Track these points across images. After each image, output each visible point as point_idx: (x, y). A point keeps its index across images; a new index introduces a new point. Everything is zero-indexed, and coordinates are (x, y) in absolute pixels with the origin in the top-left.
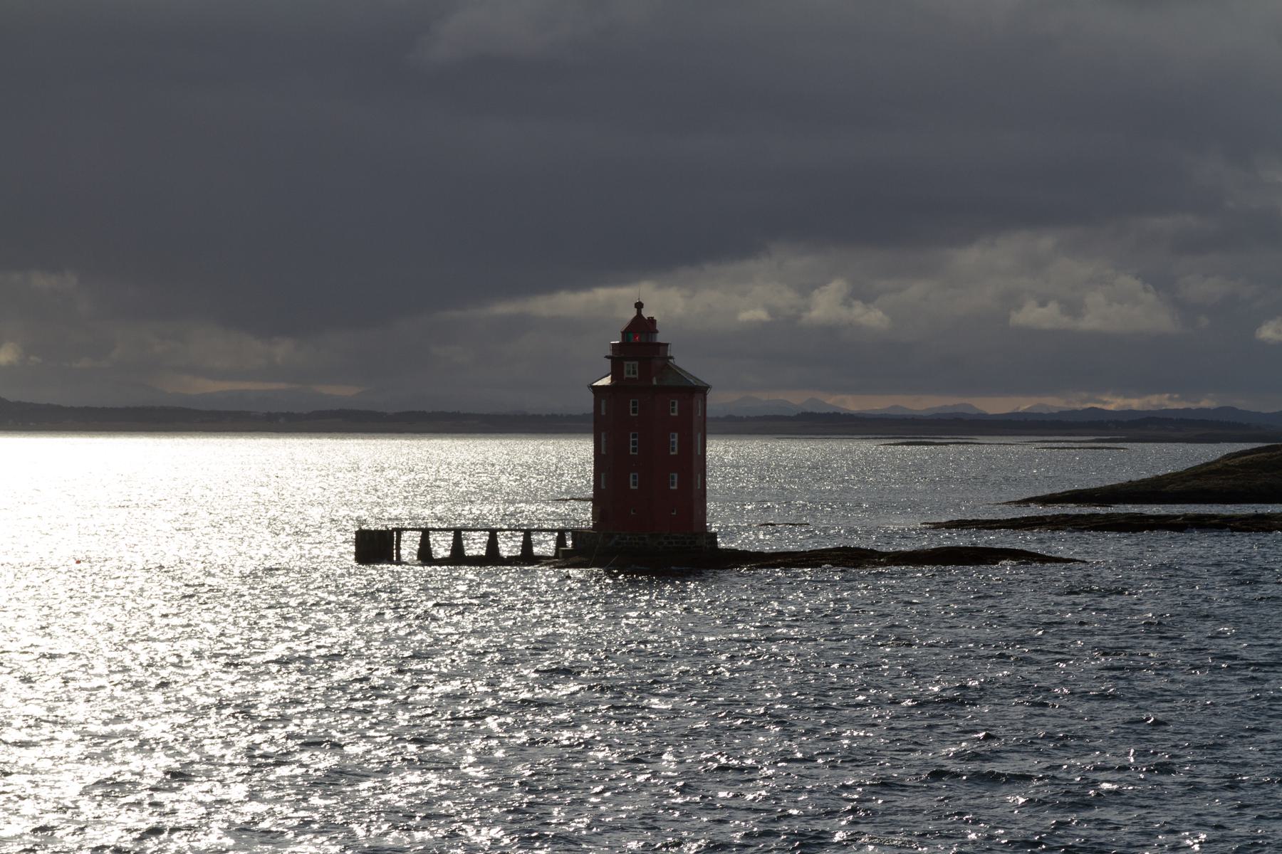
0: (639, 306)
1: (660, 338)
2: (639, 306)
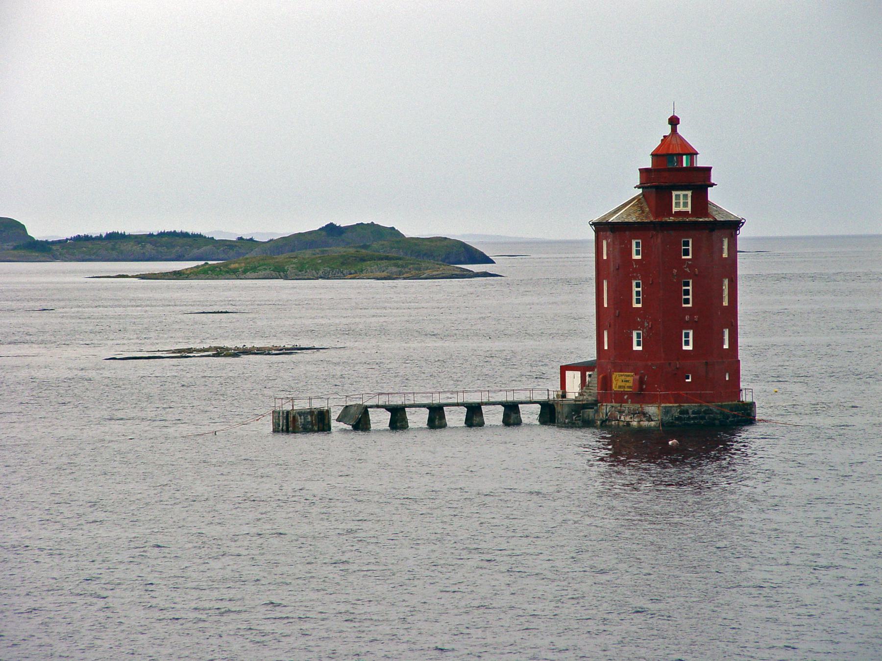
0: (674, 121)
1: (700, 162)
2: (674, 121)
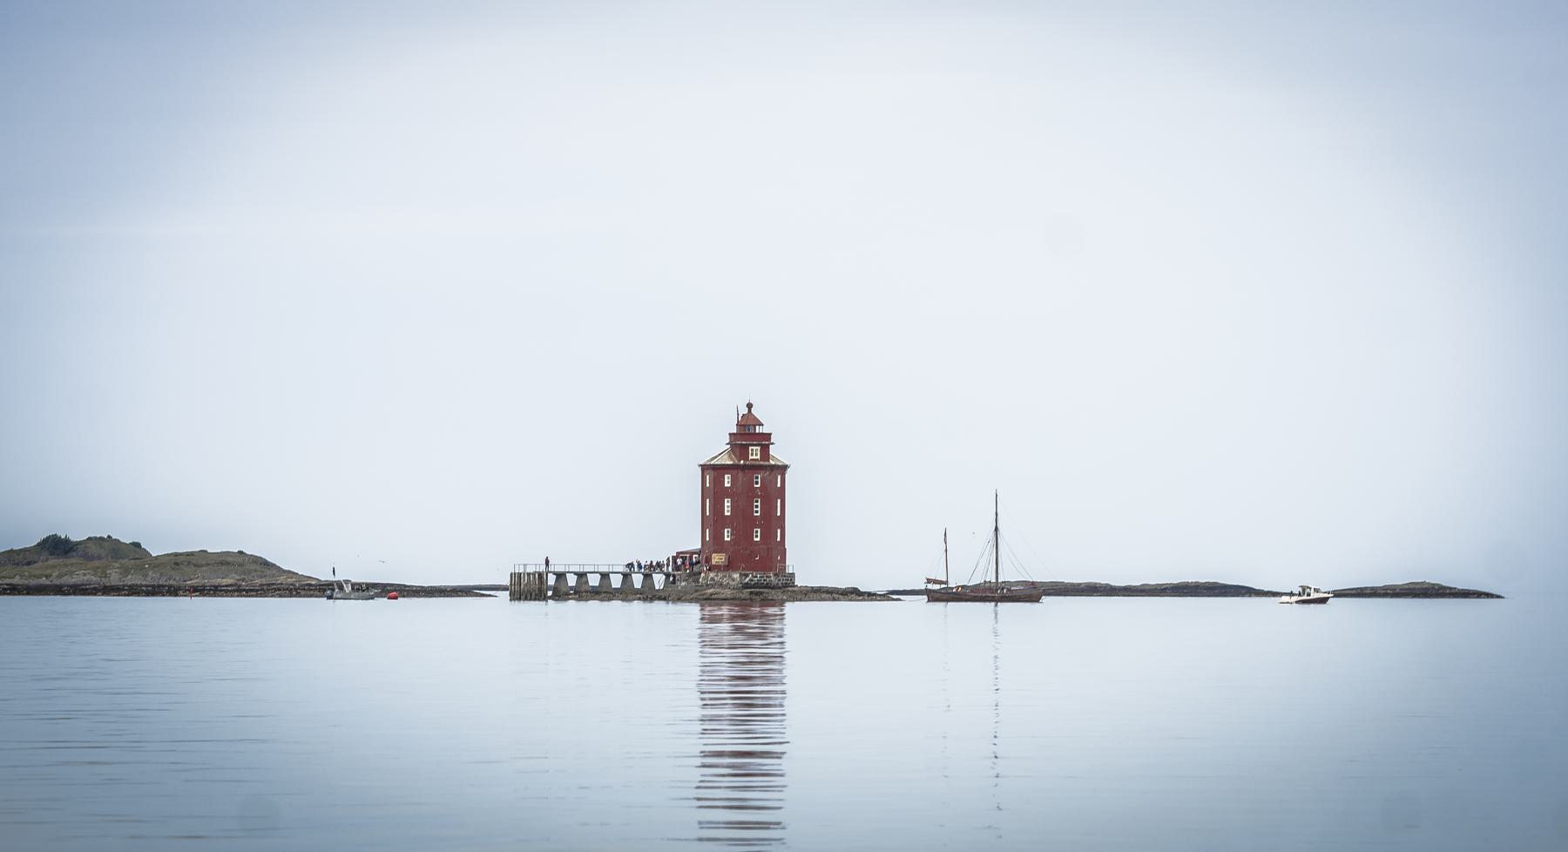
0: (750, 406)
2: (750, 406)
